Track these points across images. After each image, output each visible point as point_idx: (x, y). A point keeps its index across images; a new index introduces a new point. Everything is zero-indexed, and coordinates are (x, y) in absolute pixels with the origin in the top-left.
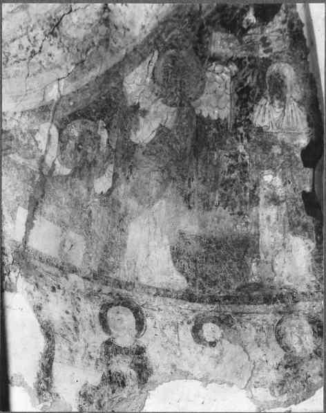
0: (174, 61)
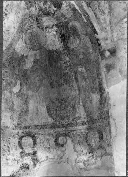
0: (31, 34)
